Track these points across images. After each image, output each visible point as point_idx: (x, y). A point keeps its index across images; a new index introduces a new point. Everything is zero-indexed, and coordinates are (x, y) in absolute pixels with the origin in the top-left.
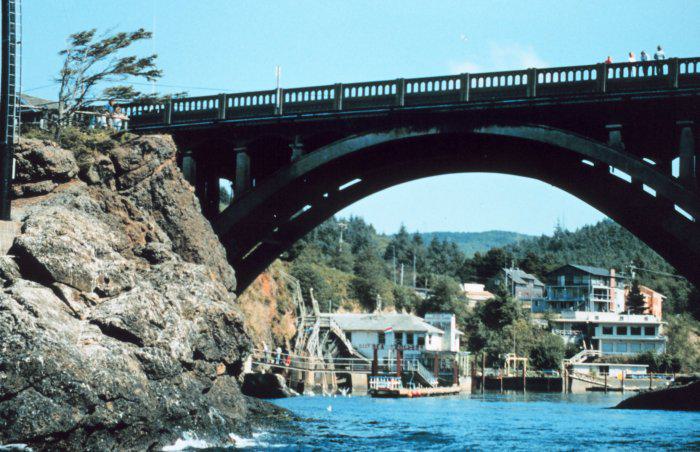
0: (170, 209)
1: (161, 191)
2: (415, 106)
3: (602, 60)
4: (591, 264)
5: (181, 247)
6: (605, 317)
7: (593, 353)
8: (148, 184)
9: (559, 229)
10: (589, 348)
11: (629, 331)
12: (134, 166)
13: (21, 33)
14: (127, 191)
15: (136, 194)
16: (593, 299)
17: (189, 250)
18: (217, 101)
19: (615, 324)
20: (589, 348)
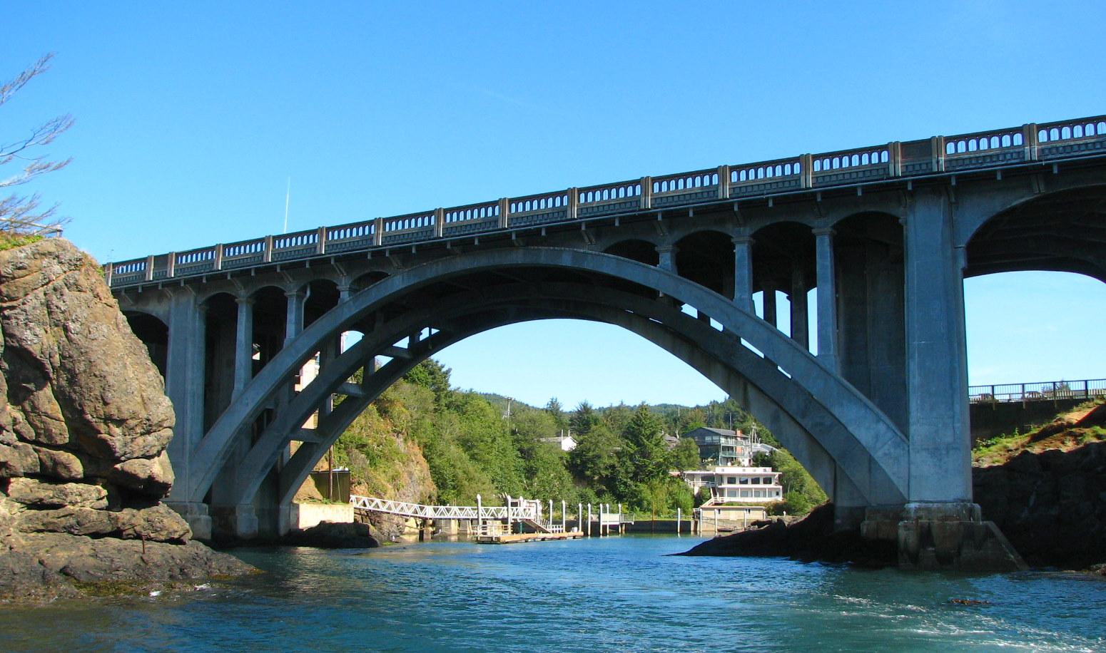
0: (71, 326)
1: (61, 304)
2: (614, 258)
3: (2, 335)
4: (711, 427)
5: (85, 371)
6: (730, 470)
7: (719, 499)
8: (41, 295)
9: (643, 403)
10: (715, 495)
11: (761, 481)
12: (21, 272)
13: (20, 87)
14: (14, 303)
15: (27, 307)
16: (721, 455)
17: (95, 375)
18: (565, 198)
19: (761, 475)
20: (715, 495)
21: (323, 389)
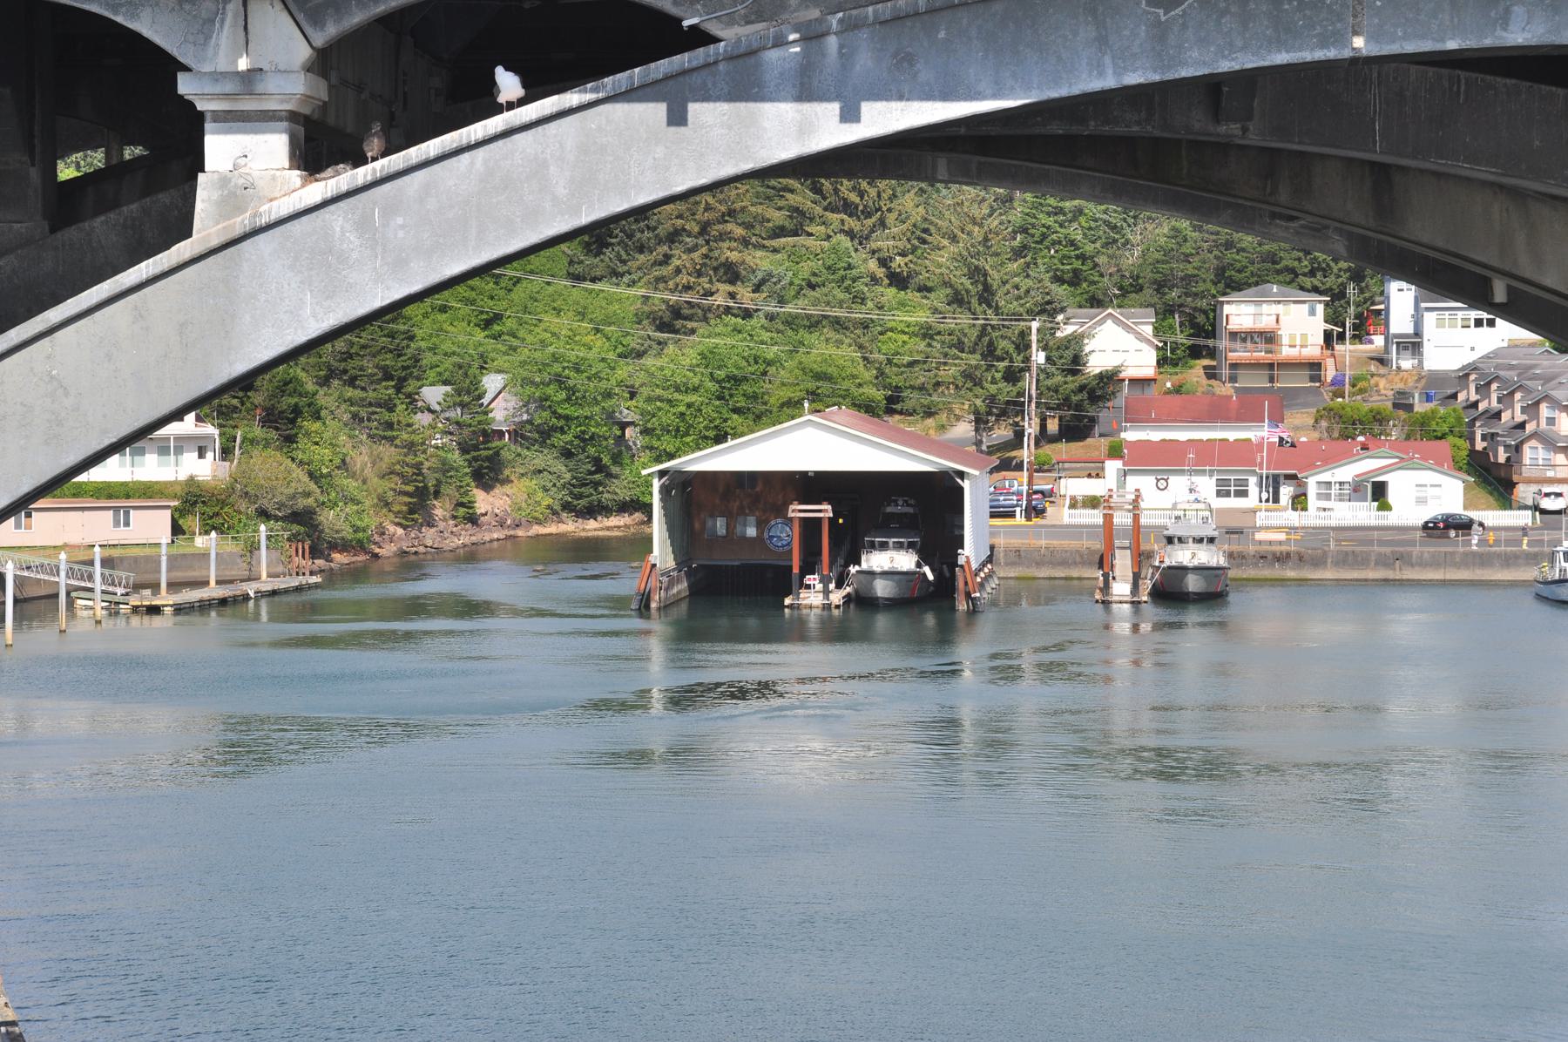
21: (882, 622)
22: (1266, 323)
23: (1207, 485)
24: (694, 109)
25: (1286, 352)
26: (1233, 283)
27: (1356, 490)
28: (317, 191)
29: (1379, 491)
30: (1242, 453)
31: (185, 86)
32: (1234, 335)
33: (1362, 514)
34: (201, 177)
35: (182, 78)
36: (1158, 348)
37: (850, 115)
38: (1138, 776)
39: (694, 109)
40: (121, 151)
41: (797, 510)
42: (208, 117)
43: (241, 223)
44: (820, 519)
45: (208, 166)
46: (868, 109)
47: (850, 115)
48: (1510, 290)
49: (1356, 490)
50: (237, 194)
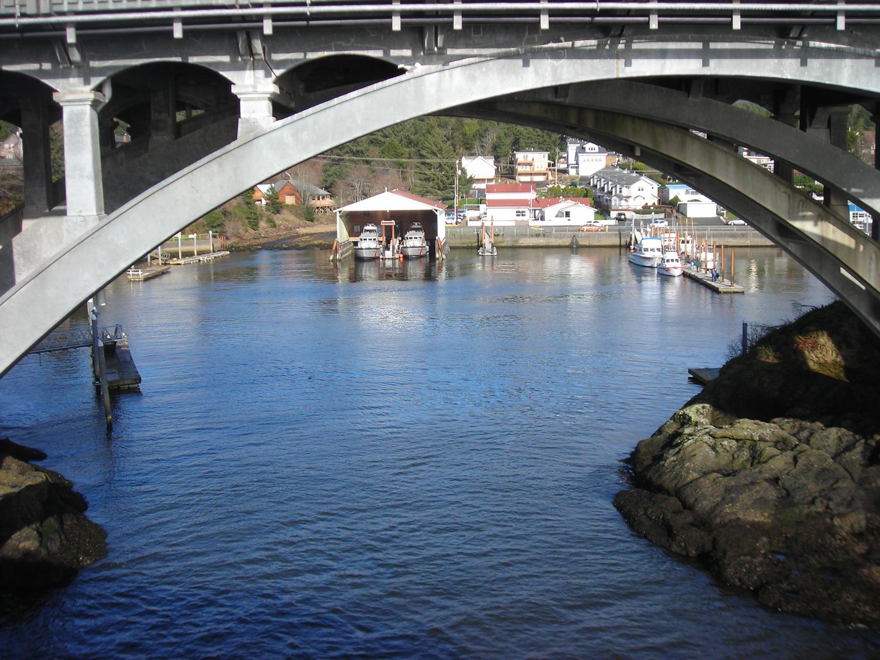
22: (529, 160)
23: (699, 62)
24: (809, 60)
25: (537, 170)
26: (517, 146)
27: (559, 215)
28: (280, 123)
29: (568, 214)
30: (524, 203)
31: (234, 90)
32: (519, 164)
33: (563, 221)
34: (239, 120)
35: (232, 86)
36: (472, 180)
37: (705, 64)
38: (169, 603)
39: (809, 60)
40: (174, 117)
41: (384, 223)
42: (242, 100)
43: (252, 135)
44: (391, 226)
45: (242, 115)
46: (712, 62)
47: (705, 64)
48: (642, 151)
49: (559, 215)
50: (253, 126)
